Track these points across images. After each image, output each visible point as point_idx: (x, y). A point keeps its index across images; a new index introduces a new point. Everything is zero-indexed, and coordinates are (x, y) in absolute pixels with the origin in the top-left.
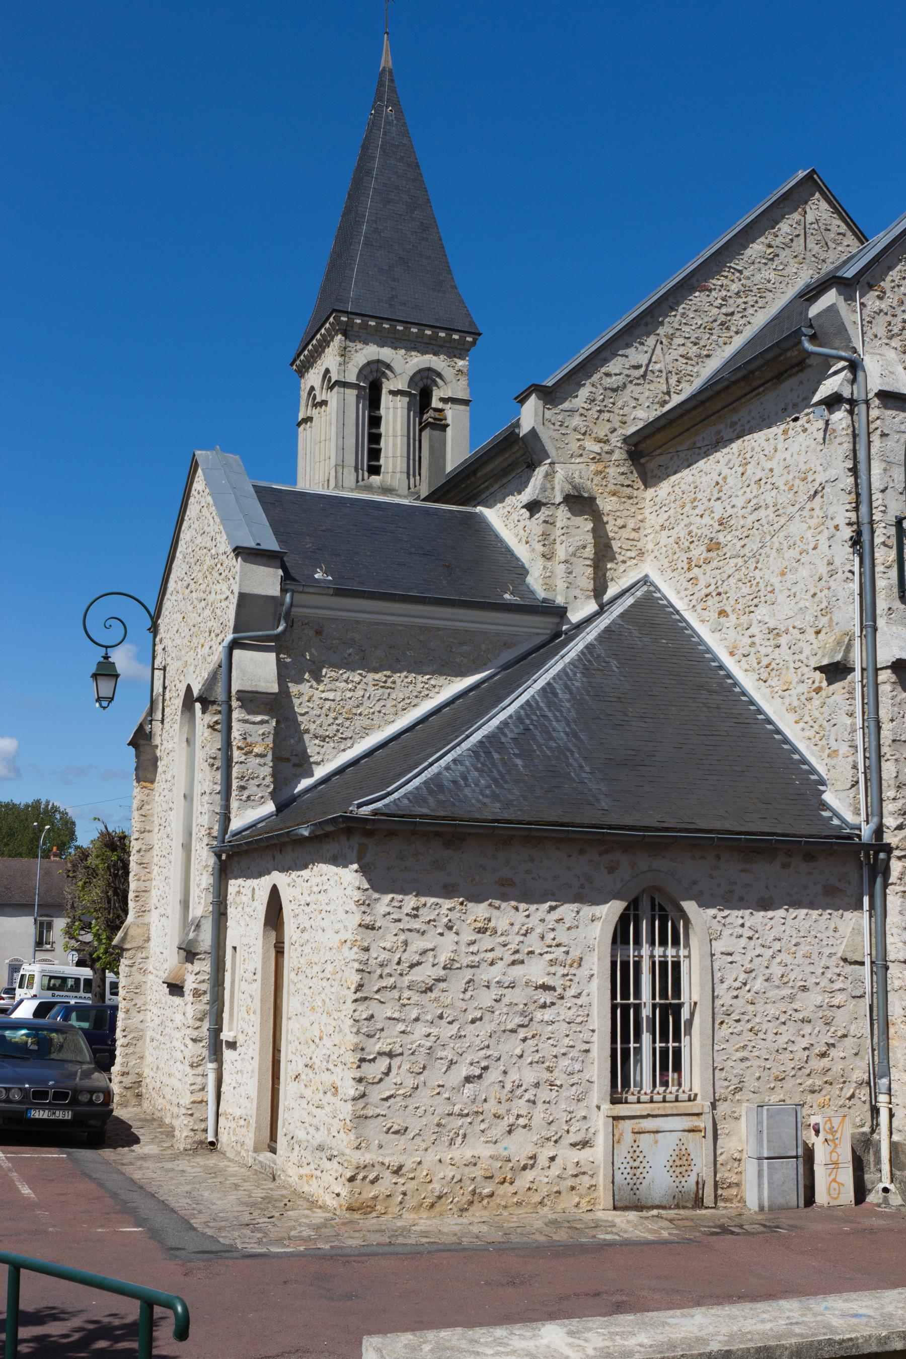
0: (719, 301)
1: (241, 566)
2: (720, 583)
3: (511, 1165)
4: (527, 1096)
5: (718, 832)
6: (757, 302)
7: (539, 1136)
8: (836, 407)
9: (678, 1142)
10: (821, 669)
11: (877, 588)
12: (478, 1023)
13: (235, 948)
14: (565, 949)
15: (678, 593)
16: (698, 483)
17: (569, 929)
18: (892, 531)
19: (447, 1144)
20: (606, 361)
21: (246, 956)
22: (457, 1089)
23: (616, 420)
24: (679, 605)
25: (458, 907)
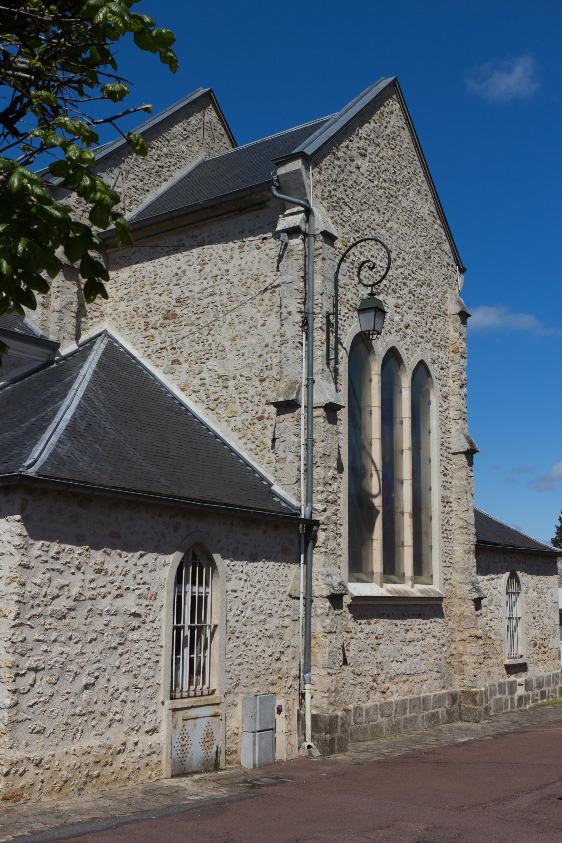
2: (174, 341)
4: (122, 697)
7: (127, 727)
8: (295, 235)
9: (207, 724)
11: (314, 356)
12: (94, 642)
14: (147, 586)
16: (159, 272)
17: (151, 571)
18: (325, 321)
25: (85, 553)
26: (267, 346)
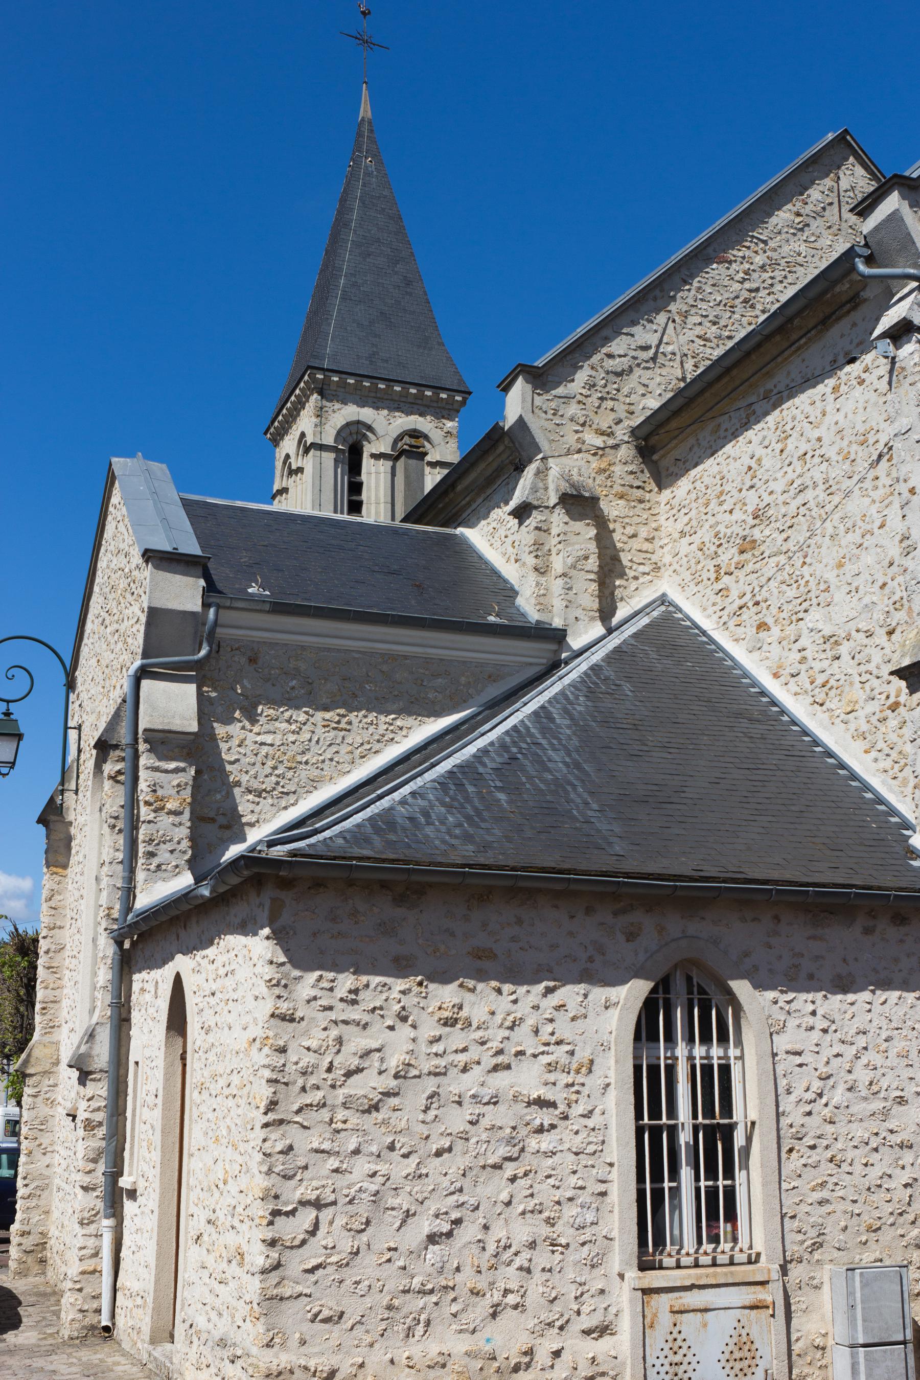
0: (741, 275)
1: (152, 573)
2: (757, 589)
3: (496, 1364)
5: (776, 882)
6: (785, 277)
7: (536, 1321)
8: (905, 338)
9: (736, 1324)
10: (900, 673)
12: (446, 1155)
13: (137, 1063)
15: (705, 610)
16: (725, 472)
19: (402, 1336)
20: (607, 340)
21: (149, 1072)
22: (416, 1254)
23: (621, 412)
24: (706, 624)
25: (416, 989)
26: (891, 564)
